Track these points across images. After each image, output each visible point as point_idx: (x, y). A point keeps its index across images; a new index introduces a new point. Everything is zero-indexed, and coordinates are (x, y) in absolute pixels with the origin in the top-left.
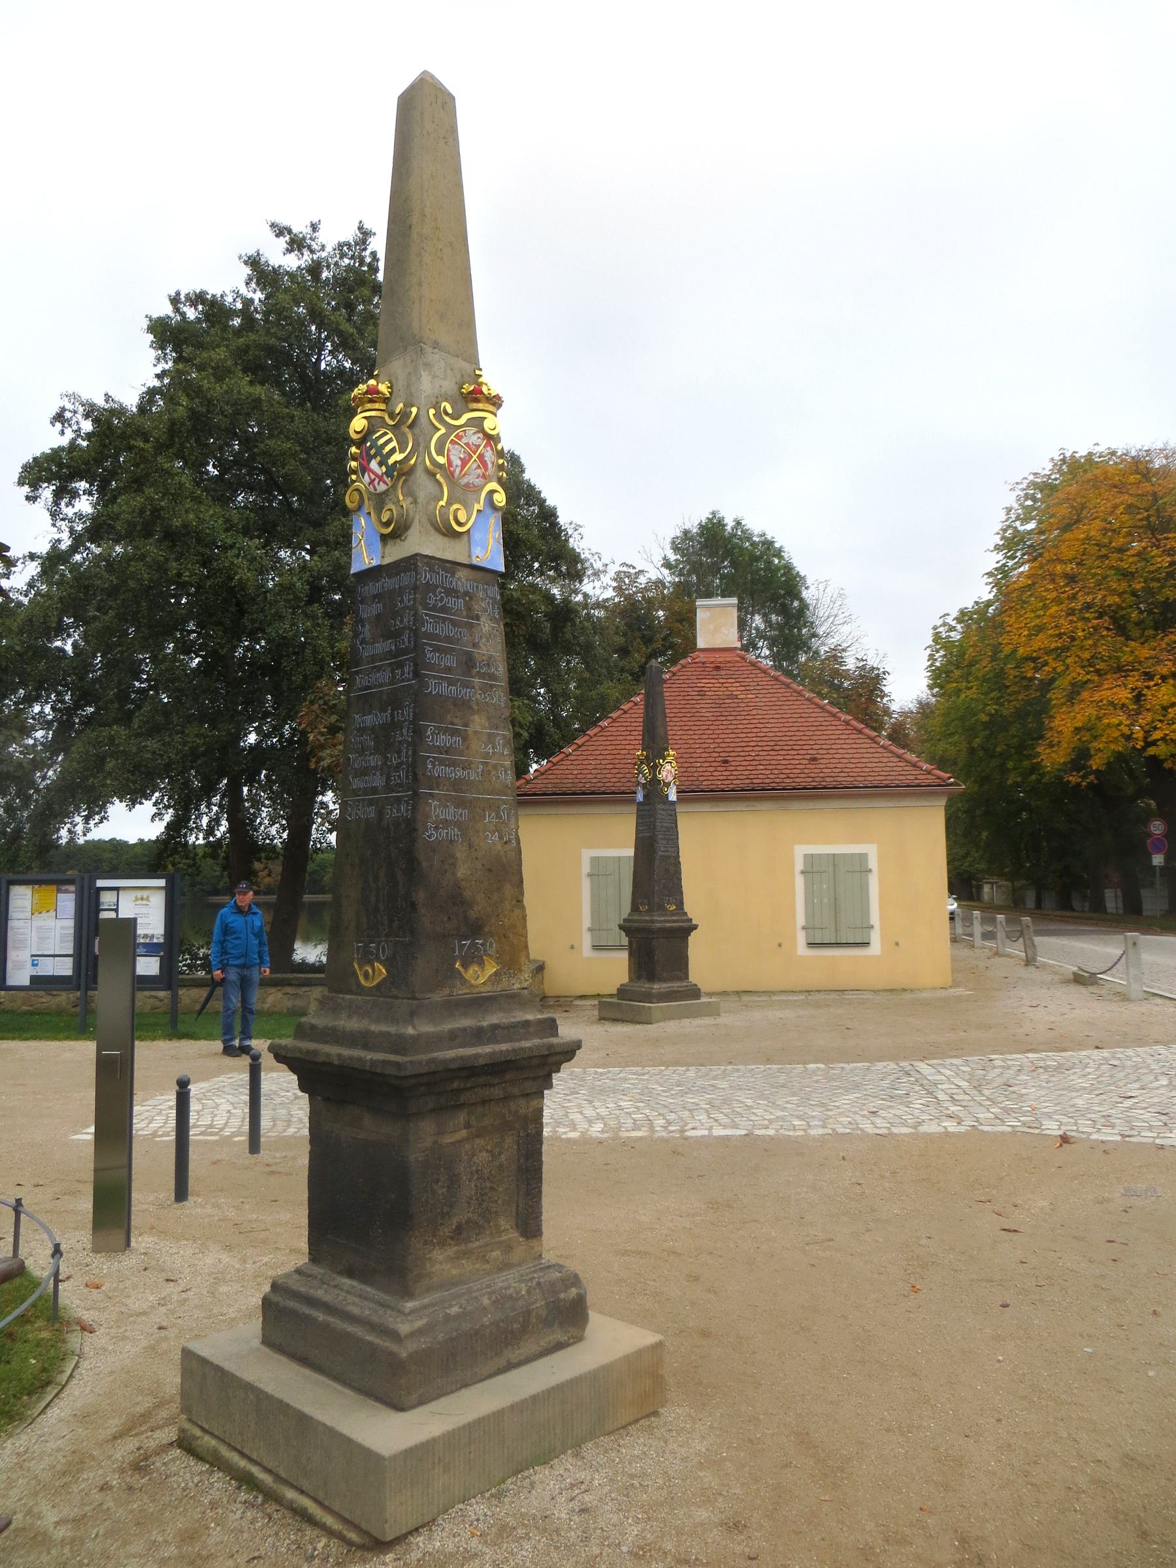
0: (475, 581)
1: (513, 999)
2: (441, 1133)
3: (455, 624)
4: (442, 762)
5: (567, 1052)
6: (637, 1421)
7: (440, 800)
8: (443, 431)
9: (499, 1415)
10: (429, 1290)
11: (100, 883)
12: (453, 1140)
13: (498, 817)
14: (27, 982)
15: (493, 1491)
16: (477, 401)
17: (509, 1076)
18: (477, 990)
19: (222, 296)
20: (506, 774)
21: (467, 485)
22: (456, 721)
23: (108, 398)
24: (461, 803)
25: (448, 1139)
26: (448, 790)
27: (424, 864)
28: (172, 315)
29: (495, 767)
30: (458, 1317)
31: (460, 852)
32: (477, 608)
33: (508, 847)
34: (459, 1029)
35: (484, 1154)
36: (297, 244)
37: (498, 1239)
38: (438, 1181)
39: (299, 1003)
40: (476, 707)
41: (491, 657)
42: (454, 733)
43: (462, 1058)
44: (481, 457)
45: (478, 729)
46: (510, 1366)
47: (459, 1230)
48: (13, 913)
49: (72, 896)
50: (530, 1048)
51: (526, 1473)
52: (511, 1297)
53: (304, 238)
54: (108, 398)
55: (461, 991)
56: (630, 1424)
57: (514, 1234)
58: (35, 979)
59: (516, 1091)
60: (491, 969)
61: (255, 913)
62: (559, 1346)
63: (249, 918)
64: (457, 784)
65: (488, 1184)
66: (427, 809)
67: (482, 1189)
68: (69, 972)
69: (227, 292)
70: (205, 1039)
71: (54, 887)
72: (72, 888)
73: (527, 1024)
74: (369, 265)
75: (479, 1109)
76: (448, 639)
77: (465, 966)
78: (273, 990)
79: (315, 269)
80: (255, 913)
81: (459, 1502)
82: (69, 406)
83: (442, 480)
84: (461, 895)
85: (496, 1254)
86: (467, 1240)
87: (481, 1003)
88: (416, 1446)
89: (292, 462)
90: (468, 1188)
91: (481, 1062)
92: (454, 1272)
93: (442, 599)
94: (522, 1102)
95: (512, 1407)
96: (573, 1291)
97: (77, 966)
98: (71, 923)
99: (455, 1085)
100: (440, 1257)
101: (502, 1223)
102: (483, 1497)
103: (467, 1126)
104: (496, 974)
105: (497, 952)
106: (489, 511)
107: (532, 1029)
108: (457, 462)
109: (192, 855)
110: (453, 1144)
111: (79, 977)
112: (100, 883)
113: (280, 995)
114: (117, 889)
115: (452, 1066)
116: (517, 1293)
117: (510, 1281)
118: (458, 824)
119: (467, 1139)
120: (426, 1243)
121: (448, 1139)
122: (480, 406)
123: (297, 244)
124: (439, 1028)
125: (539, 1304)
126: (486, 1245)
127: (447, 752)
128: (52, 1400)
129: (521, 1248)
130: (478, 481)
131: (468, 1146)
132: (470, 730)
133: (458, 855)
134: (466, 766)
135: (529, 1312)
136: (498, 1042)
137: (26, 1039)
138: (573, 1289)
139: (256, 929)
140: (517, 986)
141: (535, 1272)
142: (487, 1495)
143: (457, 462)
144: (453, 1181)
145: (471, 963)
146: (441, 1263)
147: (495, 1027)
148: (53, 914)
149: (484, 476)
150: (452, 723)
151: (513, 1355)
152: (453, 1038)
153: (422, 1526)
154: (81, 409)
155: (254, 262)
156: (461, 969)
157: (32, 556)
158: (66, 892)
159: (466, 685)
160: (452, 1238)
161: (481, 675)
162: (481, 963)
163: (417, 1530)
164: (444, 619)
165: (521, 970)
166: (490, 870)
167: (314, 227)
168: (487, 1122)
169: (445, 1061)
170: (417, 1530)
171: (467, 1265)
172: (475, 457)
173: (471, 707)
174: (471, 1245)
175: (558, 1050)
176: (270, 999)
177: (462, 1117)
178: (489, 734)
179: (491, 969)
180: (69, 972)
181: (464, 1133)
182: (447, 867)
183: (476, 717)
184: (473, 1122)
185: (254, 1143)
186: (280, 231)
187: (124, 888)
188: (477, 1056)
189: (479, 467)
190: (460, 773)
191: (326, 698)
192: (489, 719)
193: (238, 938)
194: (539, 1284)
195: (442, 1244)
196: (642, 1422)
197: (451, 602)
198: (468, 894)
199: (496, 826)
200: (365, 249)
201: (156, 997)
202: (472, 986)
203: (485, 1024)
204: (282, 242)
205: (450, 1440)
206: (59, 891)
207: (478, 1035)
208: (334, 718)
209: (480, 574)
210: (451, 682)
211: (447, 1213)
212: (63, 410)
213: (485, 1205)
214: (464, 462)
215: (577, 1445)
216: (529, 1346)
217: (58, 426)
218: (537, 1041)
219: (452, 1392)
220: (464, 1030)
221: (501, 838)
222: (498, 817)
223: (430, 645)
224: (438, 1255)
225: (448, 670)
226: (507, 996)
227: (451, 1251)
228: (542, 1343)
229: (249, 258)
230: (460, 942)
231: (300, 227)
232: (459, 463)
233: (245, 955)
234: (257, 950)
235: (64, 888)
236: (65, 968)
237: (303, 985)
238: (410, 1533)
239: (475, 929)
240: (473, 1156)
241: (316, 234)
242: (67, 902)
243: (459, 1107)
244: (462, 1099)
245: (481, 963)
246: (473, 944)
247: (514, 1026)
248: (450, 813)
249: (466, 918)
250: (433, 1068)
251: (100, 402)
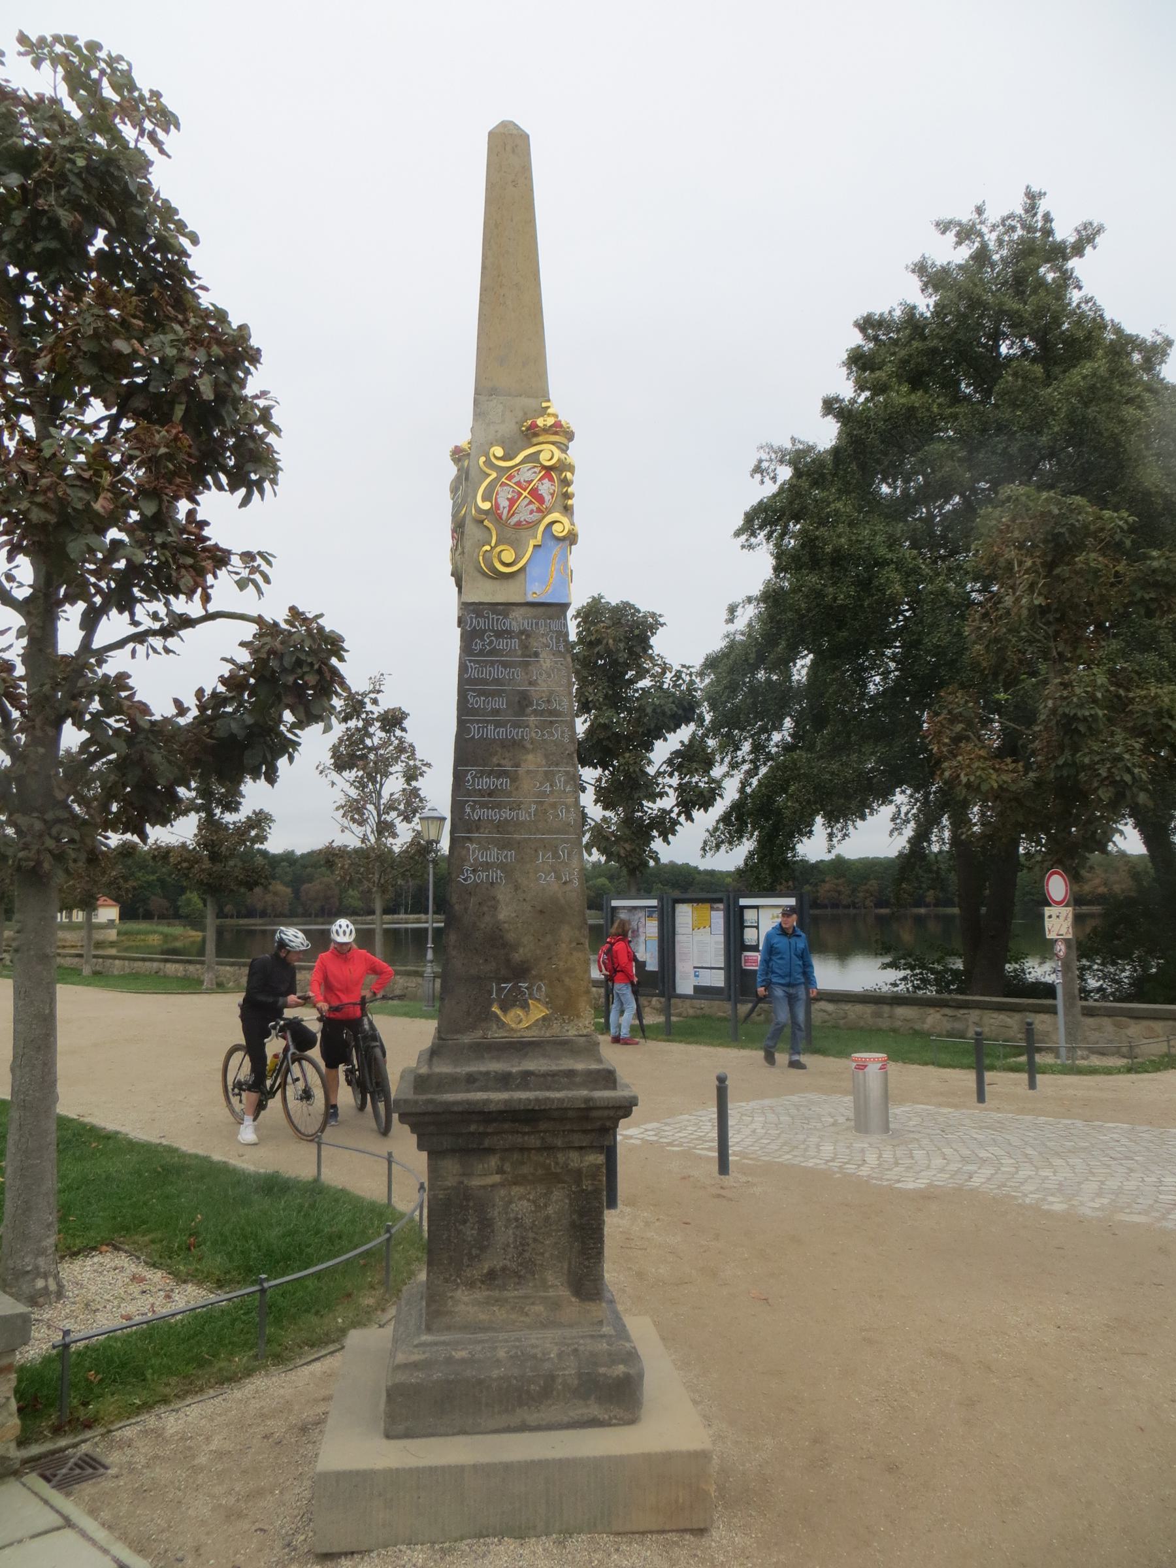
0: (535, 617)
1: (564, 1046)
2: (469, 1175)
3: (505, 665)
4: (484, 805)
5: (620, 1108)
6: (663, 1532)
7: (479, 843)
8: (494, 475)
9: (460, 1470)
10: (449, 1328)
11: (743, 902)
12: (482, 1183)
13: (556, 856)
14: (691, 992)
15: (447, 1545)
16: (536, 435)
17: (543, 1126)
18: (519, 1034)
19: (890, 312)
20: (568, 811)
21: (519, 523)
22: (503, 762)
23: (793, 440)
24: (505, 845)
25: (476, 1182)
26: (490, 833)
27: (457, 907)
28: (863, 343)
29: (554, 806)
30: (463, 1361)
31: (503, 894)
32: (535, 645)
33: (568, 888)
34: (481, 1073)
35: (525, 1203)
36: (966, 233)
37: (542, 1294)
38: (465, 1222)
39: (958, 1026)
40: (529, 746)
41: (551, 693)
42: (504, 774)
43: (468, 1102)
44: (534, 493)
45: (532, 768)
46: (523, 1428)
47: (491, 1276)
48: (679, 930)
49: (721, 914)
50: (559, 1099)
51: (488, 1540)
52: (534, 1357)
53: (974, 225)
54: (793, 440)
55: (496, 1034)
56: (651, 1532)
57: (565, 1293)
58: (697, 989)
59: (559, 1143)
60: (538, 1011)
61: (799, 936)
62: (594, 1423)
63: (793, 940)
64: (501, 826)
65: (531, 1235)
66: (464, 852)
67: (523, 1238)
68: (721, 984)
69: (895, 306)
70: (834, 1056)
71: (708, 905)
72: (721, 906)
73: (571, 1073)
74: (1043, 230)
75: (516, 1156)
76: (497, 681)
77: (505, 1009)
78: (931, 1011)
79: (982, 256)
80: (799, 936)
81: (403, 1543)
82: (765, 456)
83: (490, 525)
84: (502, 937)
85: (539, 1308)
86: (503, 1288)
87: (521, 1047)
88: (351, 1472)
89: (950, 463)
90: (504, 1235)
91: (492, 1108)
92: (482, 1317)
93: (491, 642)
94: (574, 1155)
95: (474, 1466)
96: (621, 1369)
97: (728, 979)
98: (721, 938)
99: (473, 1128)
100: (466, 1299)
101: (549, 1278)
102: (432, 1547)
103: (500, 1171)
104: (544, 1019)
105: (547, 996)
106: (551, 543)
107: (578, 1079)
108: (503, 503)
109: (935, 868)
110: (484, 1187)
111: (730, 989)
112: (743, 902)
113: (938, 1016)
114: (757, 907)
115: (455, 1109)
116: (544, 1354)
117: (546, 1343)
118: (503, 866)
119: (502, 1185)
120: (446, 1281)
121: (476, 1182)
122: (541, 439)
123: (966, 233)
124: (458, 1070)
125: (569, 1370)
126: (526, 1297)
127: (490, 795)
128: (325, 1355)
129: (572, 1308)
130: (530, 518)
131: (503, 1192)
132: (521, 771)
133: (500, 897)
134: (518, 806)
135: (551, 1378)
136: (530, 1090)
137: (689, 1043)
138: (621, 1367)
139: (799, 952)
140: (572, 1032)
141: (582, 1337)
142: (437, 1547)
143: (503, 503)
144: (486, 1224)
145: (513, 1006)
146: (466, 1304)
147: (527, 1074)
148: (708, 929)
149: (539, 510)
150: (499, 765)
151: (532, 1418)
152: (471, 1080)
153: (358, 1553)
154: (773, 456)
155: (921, 269)
156: (499, 1012)
157: (749, 600)
158: (718, 909)
159: (516, 725)
160: (483, 1282)
161: (536, 712)
162: (525, 1006)
163: (352, 1553)
164: (492, 663)
165: (578, 1016)
166: (541, 912)
167: (980, 211)
168: (525, 1170)
169: (447, 1103)
170: (352, 1553)
171: (500, 1314)
172: (525, 494)
173: (523, 747)
174: (506, 1294)
175: (598, 1104)
176: (930, 1021)
177: (493, 1161)
178: (546, 773)
179: (538, 1011)
180: (721, 984)
181: (497, 1178)
182: (485, 909)
183: (530, 757)
184: (507, 1167)
185: (723, 1165)
186: (944, 227)
187: (763, 906)
188: (487, 1102)
189: (531, 502)
190: (506, 814)
191: (950, 707)
192: (546, 756)
193: (781, 958)
194: (576, 1350)
195: (471, 1285)
196: (668, 1536)
197: (501, 644)
198: (511, 937)
199: (551, 866)
200: (1035, 214)
201: (825, 1011)
202: (512, 1029)
203: (514, 1070)
204: (951, 236)
205: (394, 1475)
206: (712, 909)
207: (504, 1081)
208: (959, 727)
209: (541, 610)
210: (498, 724)
211: (477, 1256)
212: (760, 461)
213: (527, 1255)
214: (512, 502)
215: (568, 1532)
216: (552, 1412)
217: (758, 476)
218: (584, 1093)
219: (447, 1435)
220: (487, 1073)
221: (558, 878)
222: (556, 856)
223: (474, 690)
224: (462, 1295)
225: (496, 712)
226: (555, 1043)
227: (481, 1294)
228: (571, 1414)
229: (915, 265)
230: (498, 984)
231: (966, 216)
232: (507, 503)
233: (790, 975)
234: (800, 970)
235: (716, 906)
236: (717, 979)
237: (961, 1008)
238: (346, 1554)
239: (520, 972)
240: (511, 1202)
241: (984, 216)
242: (718, 918)
243: (490, 1151)
244: (487, 1143)
245: (525, 1006)
246: (515, 987)
247: (554, 1074)
248: (493, 855)
249: (508, 961)
250: (430, 1108)
251: (788, 445)
